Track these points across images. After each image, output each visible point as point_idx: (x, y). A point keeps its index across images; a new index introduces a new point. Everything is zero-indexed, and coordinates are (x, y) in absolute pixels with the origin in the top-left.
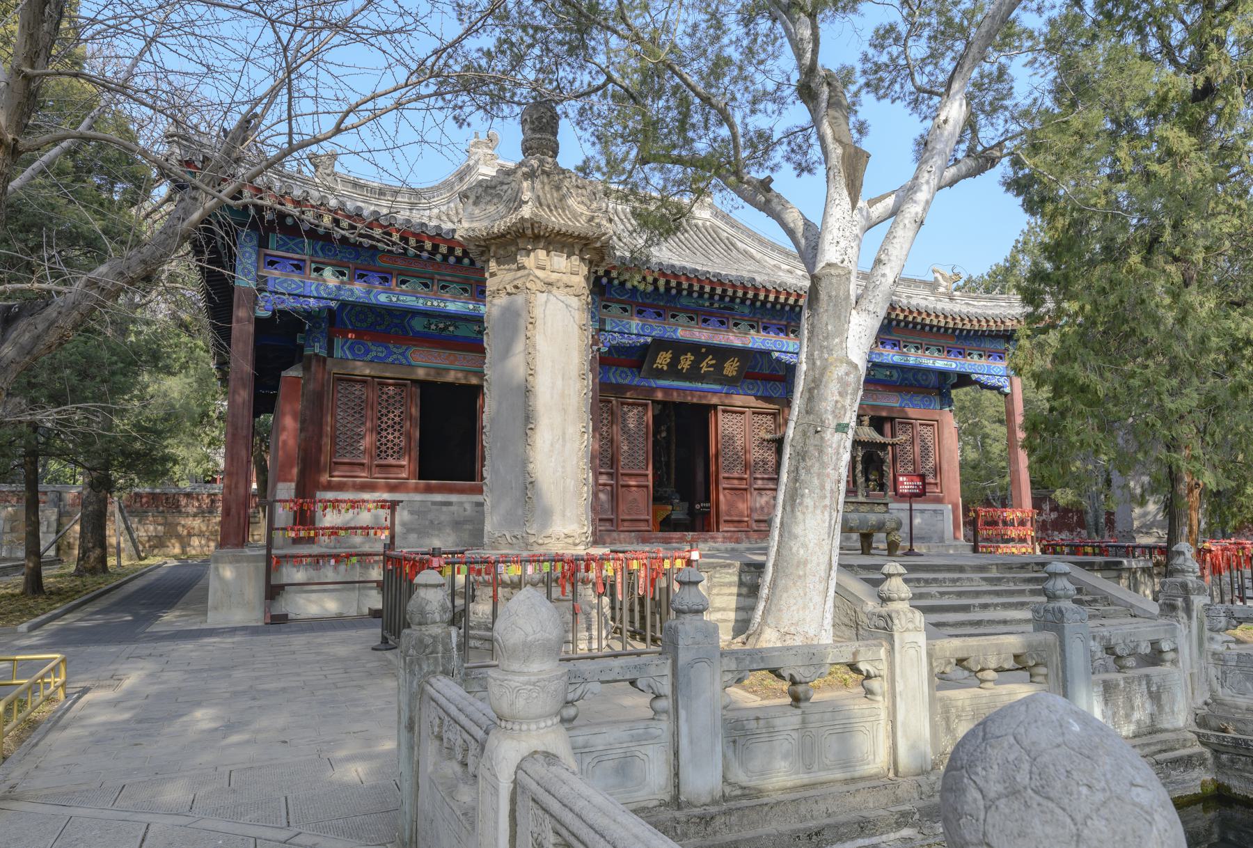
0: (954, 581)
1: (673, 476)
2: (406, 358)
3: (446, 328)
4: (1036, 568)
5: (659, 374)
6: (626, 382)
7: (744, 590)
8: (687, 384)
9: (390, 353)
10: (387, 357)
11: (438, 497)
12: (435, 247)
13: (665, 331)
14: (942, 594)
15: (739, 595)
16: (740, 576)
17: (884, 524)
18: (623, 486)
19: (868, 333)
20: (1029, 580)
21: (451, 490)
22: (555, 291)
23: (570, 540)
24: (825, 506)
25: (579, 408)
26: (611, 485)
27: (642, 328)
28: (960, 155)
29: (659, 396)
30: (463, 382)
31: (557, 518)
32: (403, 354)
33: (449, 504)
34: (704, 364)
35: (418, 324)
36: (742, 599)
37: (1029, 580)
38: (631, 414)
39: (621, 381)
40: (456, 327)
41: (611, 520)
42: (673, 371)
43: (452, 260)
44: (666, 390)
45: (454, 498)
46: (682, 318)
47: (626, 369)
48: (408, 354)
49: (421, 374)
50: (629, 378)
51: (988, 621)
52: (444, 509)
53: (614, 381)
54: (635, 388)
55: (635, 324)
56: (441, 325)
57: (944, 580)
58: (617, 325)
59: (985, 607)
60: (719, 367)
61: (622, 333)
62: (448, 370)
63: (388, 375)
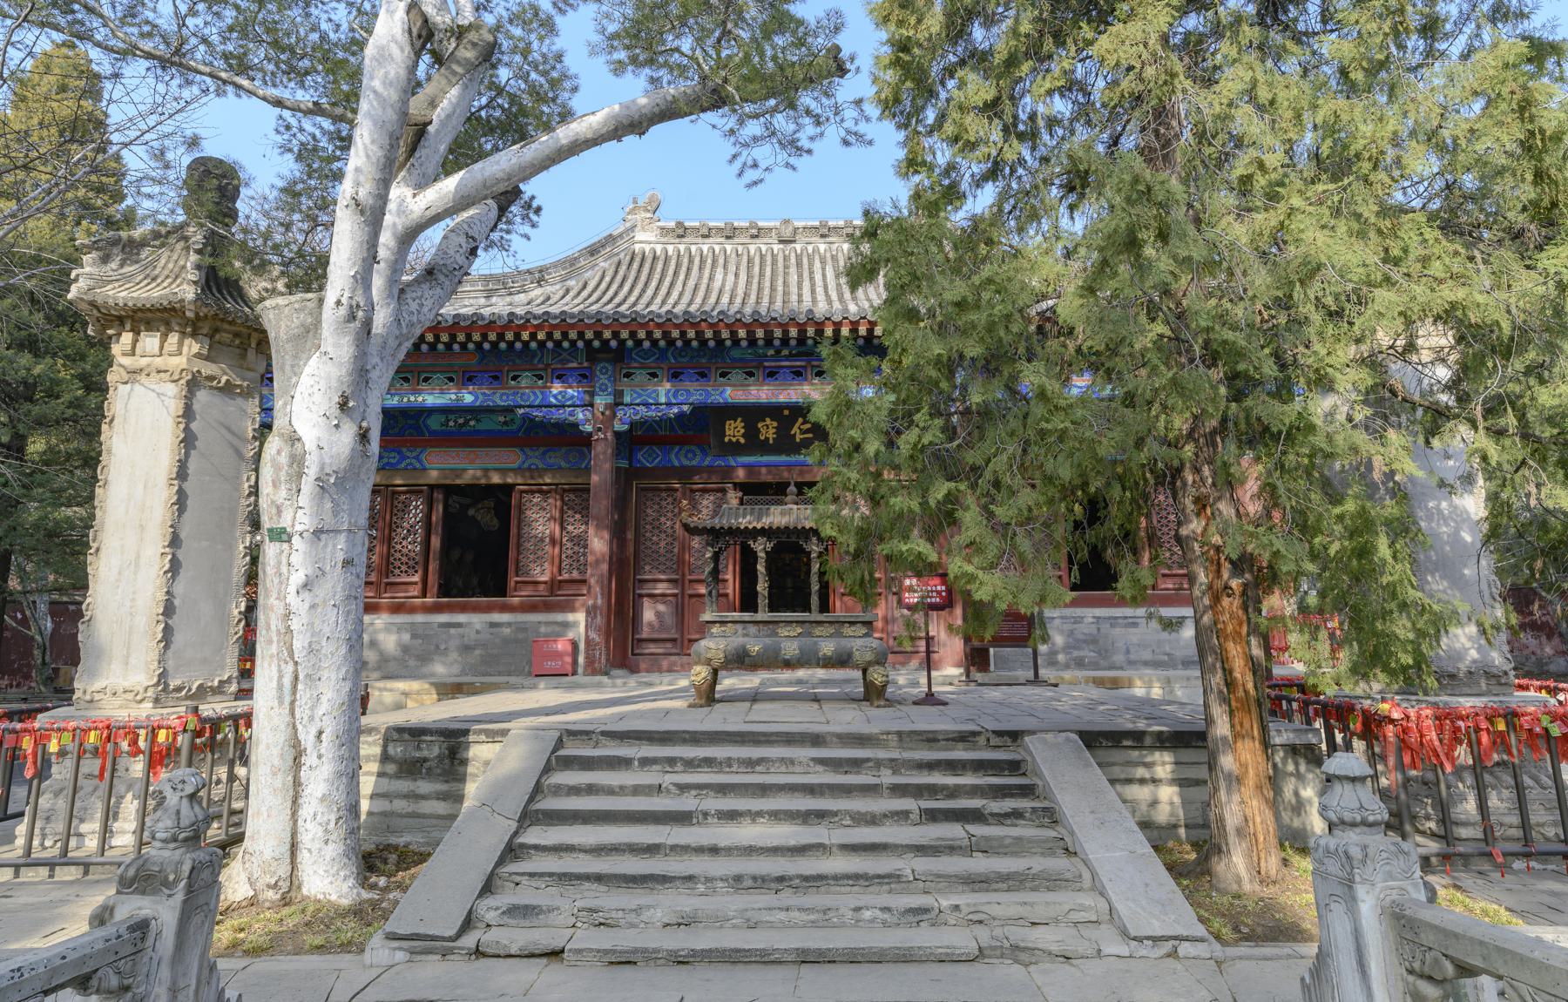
0: (751, 764)
1: (814, 579)
2: (420, 462)
3: (467, 422)
4: (995, 741)
5: (736, 449)
6: (694, 463)
7: (391, 768)
8: (783, 458)
9: (404, 458)
10: (399, 462)
11: (443, 618)
12: (453, 337)
13: (708, 394)
14: (683, 788)
15: (380, 775)
16: (385, 747)
17: (850, 655)
18: (691, 596)
19: (323, 385)
20: (980, 766)
21: (464, 609)
22: (143, 378)
23: (130, 696)
24: (272, 656)
25: (164, 522)
26: (675, 595)
27: (675, 396)
28: (195, 90)
29: (741, 474)
30: (483, 481)
31: (116, 666)
32: (417, 458)
33: (459, 625)
34: (795, 430)
35: (434, 423)
36: (385, 781)
37: (980, 766)
38: (705, 502)
39: (686, 463)
40: (478, 421)
41: (674, 640)
42: (753, 443)
43: (456, 347)
44: (749, 467)
45: (461, 618)
46: (737, 376)
47: (693, 448)
48: (423, 457)
49: (433, 476)
50: (698, 459)
51: (674, 848)
52: (453, 631)
53: (676, 464)
54: (711, 470)
55: (663, 390)
56: (461, 421)
57: (729, 762)
58: (640, 395)
59: (732, 816)
60: (751, 432)
61: (647, 405)
62: (464, 470)
63: (399, 482)
